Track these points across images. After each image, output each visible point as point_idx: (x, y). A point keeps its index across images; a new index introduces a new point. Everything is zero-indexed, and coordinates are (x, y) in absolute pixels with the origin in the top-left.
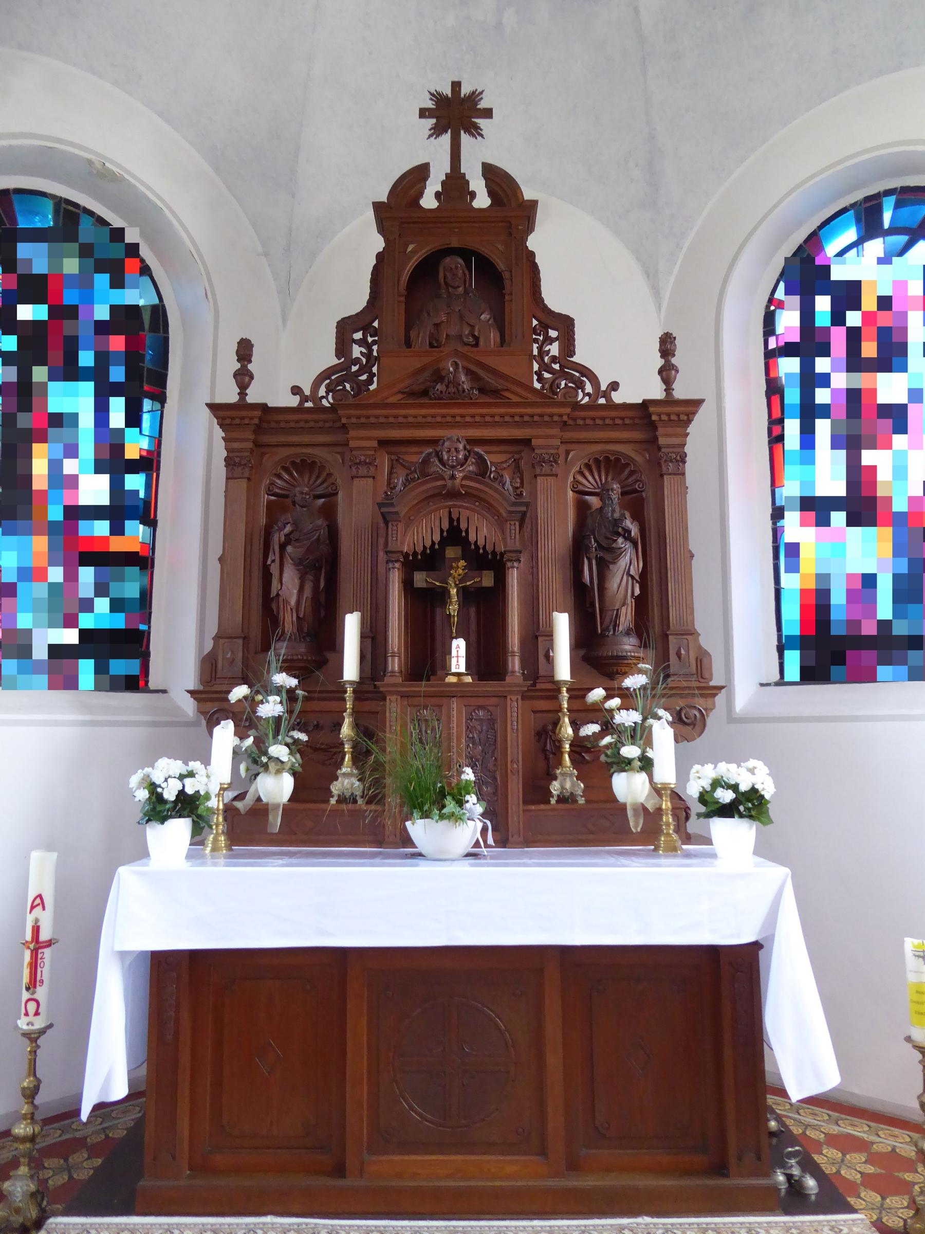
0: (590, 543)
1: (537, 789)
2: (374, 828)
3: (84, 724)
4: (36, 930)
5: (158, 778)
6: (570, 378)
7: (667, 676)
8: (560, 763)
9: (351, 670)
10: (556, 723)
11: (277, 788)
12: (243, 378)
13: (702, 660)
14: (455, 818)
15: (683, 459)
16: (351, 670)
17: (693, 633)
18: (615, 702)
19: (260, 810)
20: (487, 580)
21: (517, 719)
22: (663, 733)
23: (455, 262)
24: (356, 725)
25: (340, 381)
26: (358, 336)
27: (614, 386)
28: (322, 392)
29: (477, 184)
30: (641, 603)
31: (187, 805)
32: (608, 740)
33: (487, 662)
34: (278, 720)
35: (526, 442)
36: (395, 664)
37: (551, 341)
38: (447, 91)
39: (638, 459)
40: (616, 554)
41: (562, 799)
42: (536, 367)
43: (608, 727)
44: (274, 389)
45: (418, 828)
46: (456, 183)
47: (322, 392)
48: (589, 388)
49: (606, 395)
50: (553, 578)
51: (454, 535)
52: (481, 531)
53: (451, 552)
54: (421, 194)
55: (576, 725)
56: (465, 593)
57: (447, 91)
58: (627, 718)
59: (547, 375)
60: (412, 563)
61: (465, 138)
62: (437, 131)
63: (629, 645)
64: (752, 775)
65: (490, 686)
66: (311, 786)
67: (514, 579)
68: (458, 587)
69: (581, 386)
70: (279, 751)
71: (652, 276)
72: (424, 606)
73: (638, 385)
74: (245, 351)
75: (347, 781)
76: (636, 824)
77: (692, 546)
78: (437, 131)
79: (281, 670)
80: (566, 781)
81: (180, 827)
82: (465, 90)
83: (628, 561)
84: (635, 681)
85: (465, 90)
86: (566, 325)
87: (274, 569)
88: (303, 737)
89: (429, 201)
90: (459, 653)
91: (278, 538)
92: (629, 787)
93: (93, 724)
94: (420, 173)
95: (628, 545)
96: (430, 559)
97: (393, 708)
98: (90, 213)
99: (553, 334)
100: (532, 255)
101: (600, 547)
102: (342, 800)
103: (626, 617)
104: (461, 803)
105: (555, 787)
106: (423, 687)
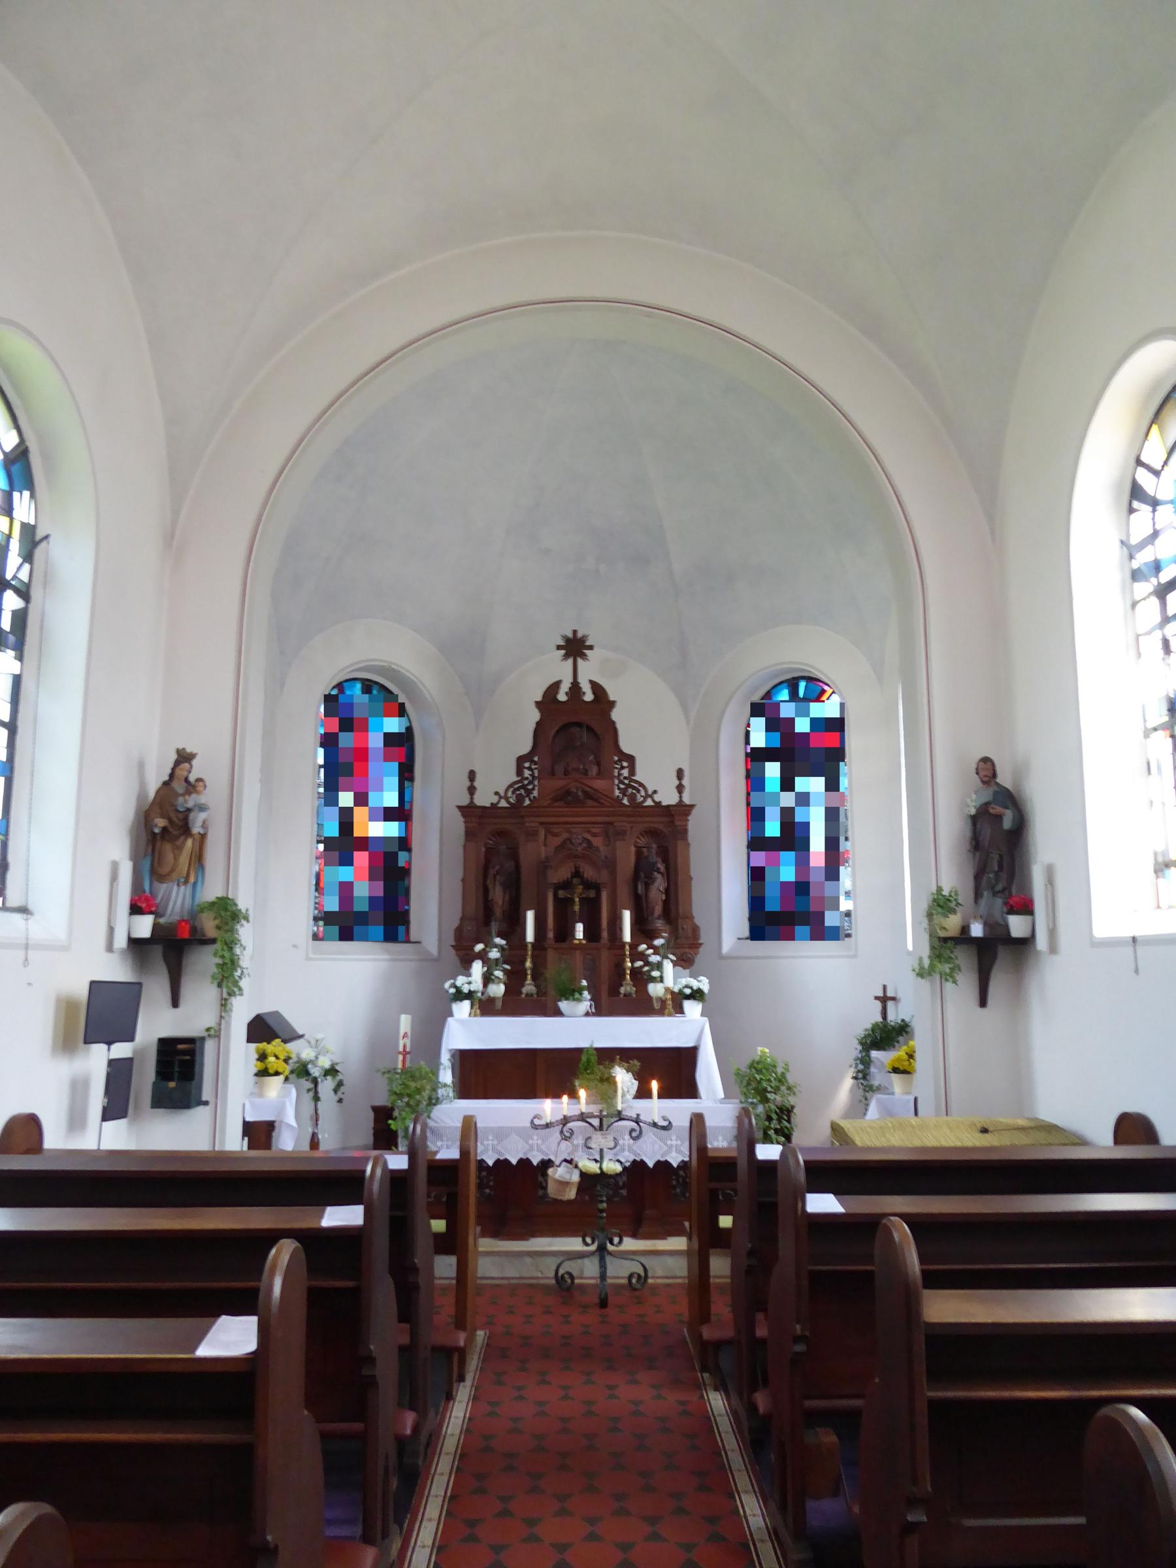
0: (642, 872)
1: (614, 991)
2: (544, 1006)
3: (386, 960)
4: (405, 1046)
5: (458, 983)
6: (634, 788)
7: (677, 938)
8: (625, 978)
9: (530, 937)
10: (624, 961)
11: (498, 990)
12: (472, 790)
13: (696, 930)
14: (579, 1000)
15: (685, 831)
16: (530, 937)
17: (691, 917)
18: (651, 951)
19: (491, 1000)
20: (592, 894)
21: (605, 957)
22: (668, 966)
23: (576, 730)
24: (533, 962)
25: (518, 789)
26: (527, 765)
27: (655, 792)
28: (510, 794)
29: (586, 688)
30: (666, 903)
31: (470, 995)
32: (646, 969)
33: (592, 933)
34: (497, 960)
35: (611, 823)
36: (551, 935)
37: (623, 768)
38: (570, 635)
39: (665, 830)
40: (653, 880)
41: (625, 995)
42: (616, 782)
43: (647, 963)
44: (484, 799)
45: (563, 1005)
46: (575, 688)
47: (510, 794)
48: (643, 793)
49: (651, 796)
50: (624, 892)
51: (577, 874)
52: (589, 872)
53: (575, 881)
54: (557, 693)
55: (632, 962)
56: (581, 900)
57: (570, 635)
58: (655, 959)
59: (622, 786)
60: (558, 887)
61: (580, 661)
62: (566, 656)
63: (659, 924)
64: (704, 984)
65: (594, 945)
66: (513, 986)
67: (604, 895)
68: (579, 900)
69: (638, 791)
70: (499, 973)
71: (685, 707)
72: (563, 906)
73: (668, 797)
74: (472, 775)
75: (529, 987)
76: (657, 1006)
77: (692, 874)
78: (566, 656)
79: (498, 936)
80: (627, 988)
81: (466, 1004)
82: (579, 635)
83: (660, 883)
84: (658, 942)
85: (579, 635)
86: (631, 759)
87: (490, 887)
88: (508, 967)
89: (562, 697)
90: (579, 930)
91: (492, 872)
92: (655, 990)
93: (394, 960)
94: (555, 686)
95: (659, 876)
96: (566, 885)
97: (551, 955)
98: (376, 683)
99: (625, 764)
100: (614, 723)
101: (646, 877)
102: (527, 995)
103: (658, 910)
104: (581, 994)
105: (622, 990)
106: (564, 945)
